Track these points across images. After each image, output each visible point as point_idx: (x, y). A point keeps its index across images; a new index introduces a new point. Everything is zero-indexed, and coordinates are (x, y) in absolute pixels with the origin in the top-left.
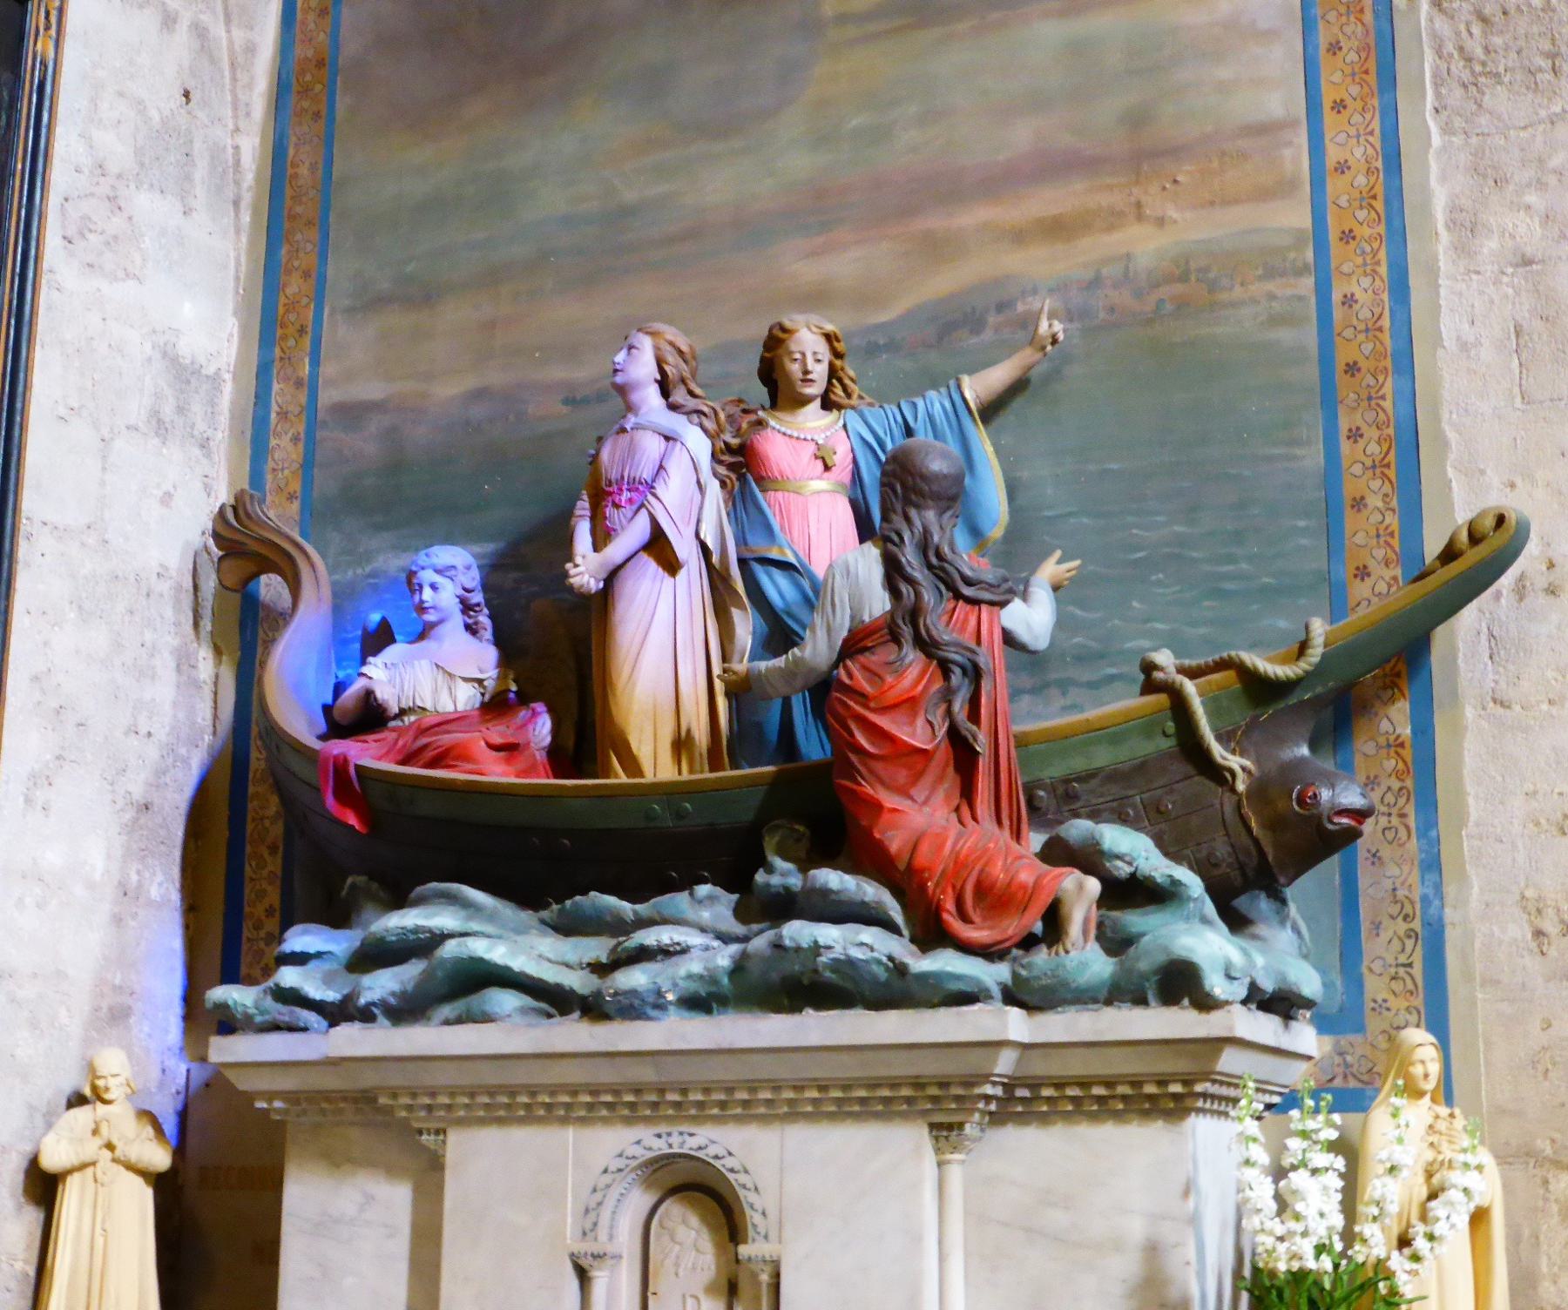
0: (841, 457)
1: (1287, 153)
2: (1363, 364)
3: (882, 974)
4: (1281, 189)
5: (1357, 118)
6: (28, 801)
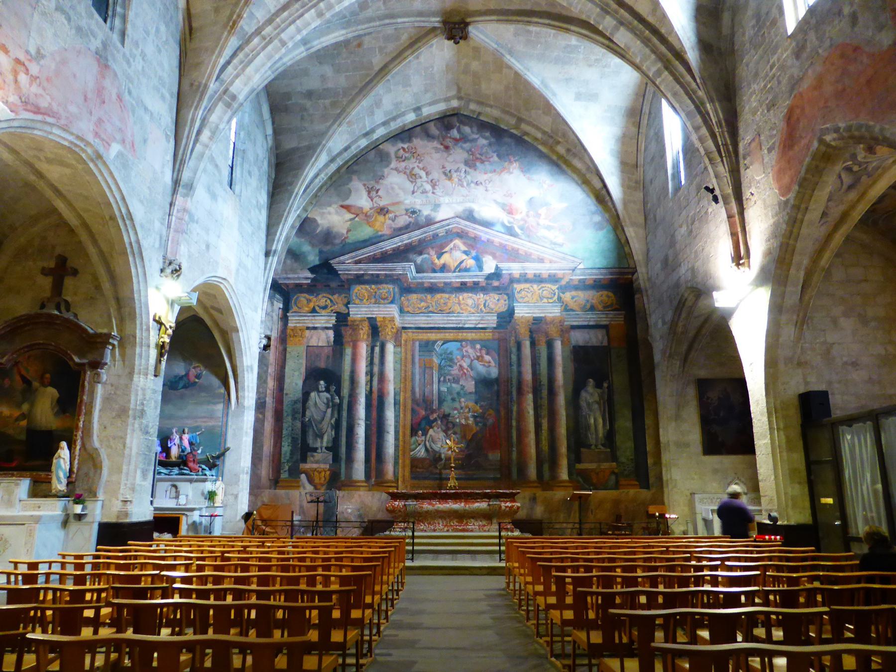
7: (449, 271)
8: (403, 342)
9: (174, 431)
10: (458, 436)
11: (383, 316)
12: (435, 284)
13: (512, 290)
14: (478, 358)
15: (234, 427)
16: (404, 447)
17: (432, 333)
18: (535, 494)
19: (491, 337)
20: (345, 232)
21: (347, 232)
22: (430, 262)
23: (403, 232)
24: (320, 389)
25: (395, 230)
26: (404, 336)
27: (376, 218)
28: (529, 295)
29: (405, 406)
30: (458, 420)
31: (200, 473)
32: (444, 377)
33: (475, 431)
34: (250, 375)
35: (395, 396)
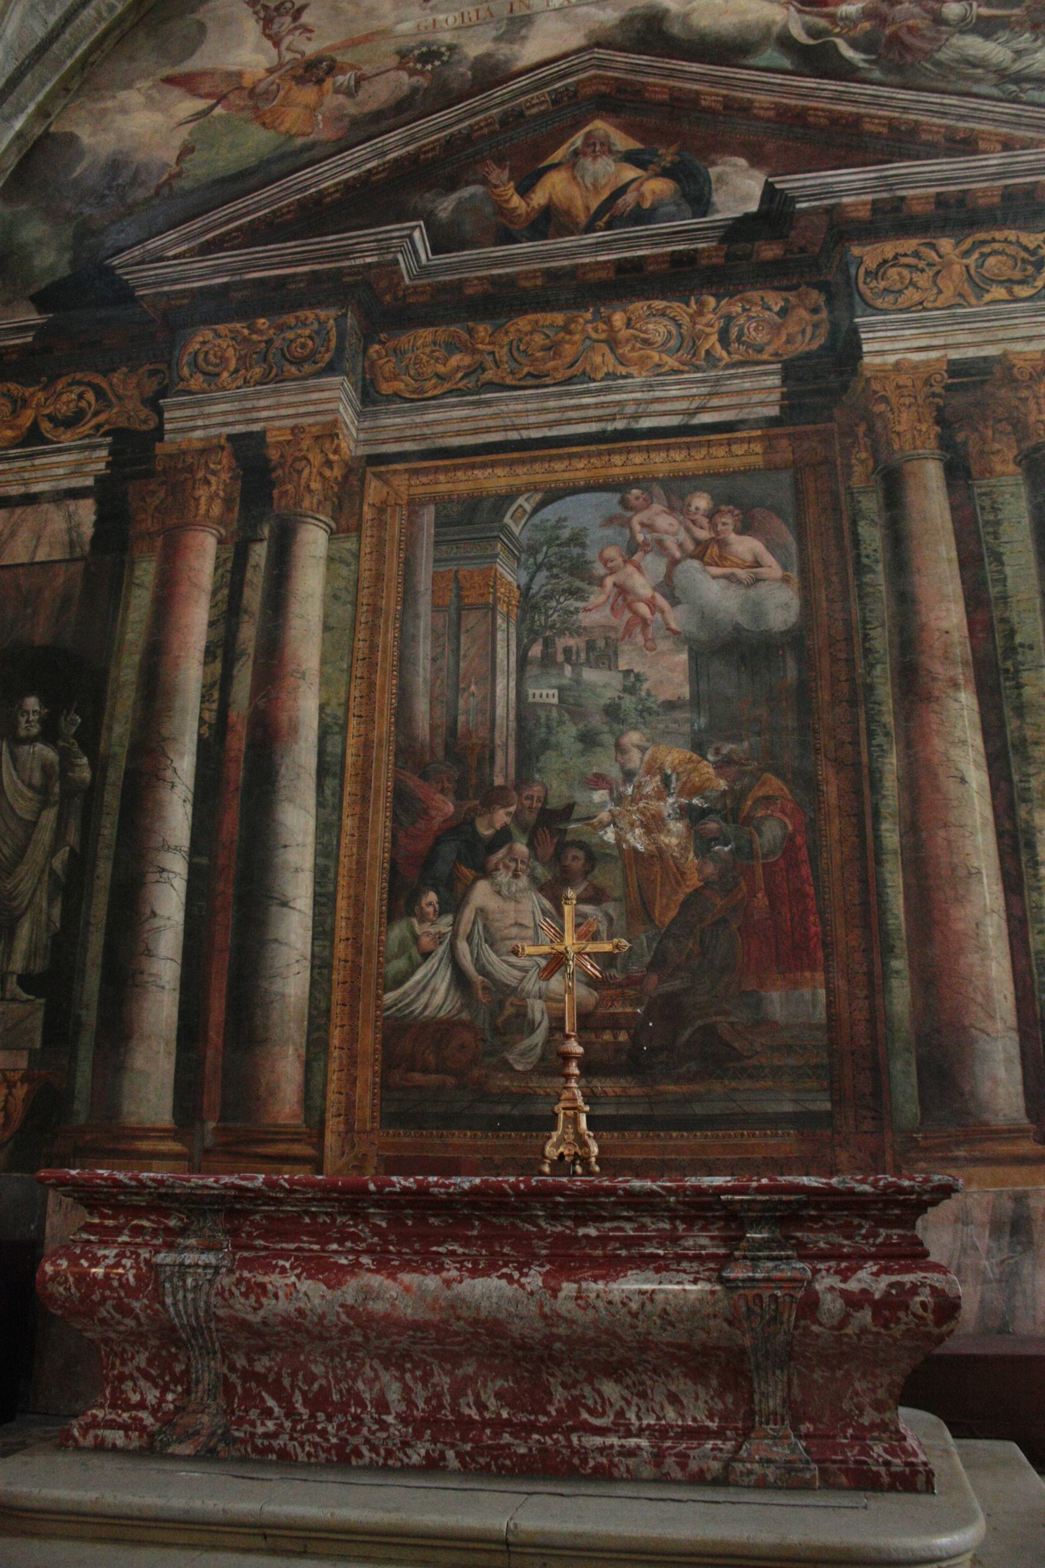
7: (565, 230)
8: (368, 513)
10: (611, 908)
11: (289, 423)
12: (510, 281)
13: (846, 272)
14: (700, 551)
16: (356, 969)
17: (493, 465)
18: (1019, 1199)
19: (757, 461)
20: (170, 156)
21: (179, 160)
22: (488, 209)
23: (384, 124)
24: (23, 733)
25: (355, 122)
26: (374, 491)
27: (286, 96)
28: (923, 280)
29: (365, 781)
30: (610, 836)
32: (548, 643)
33: (694, 881)
35: (322, 738)
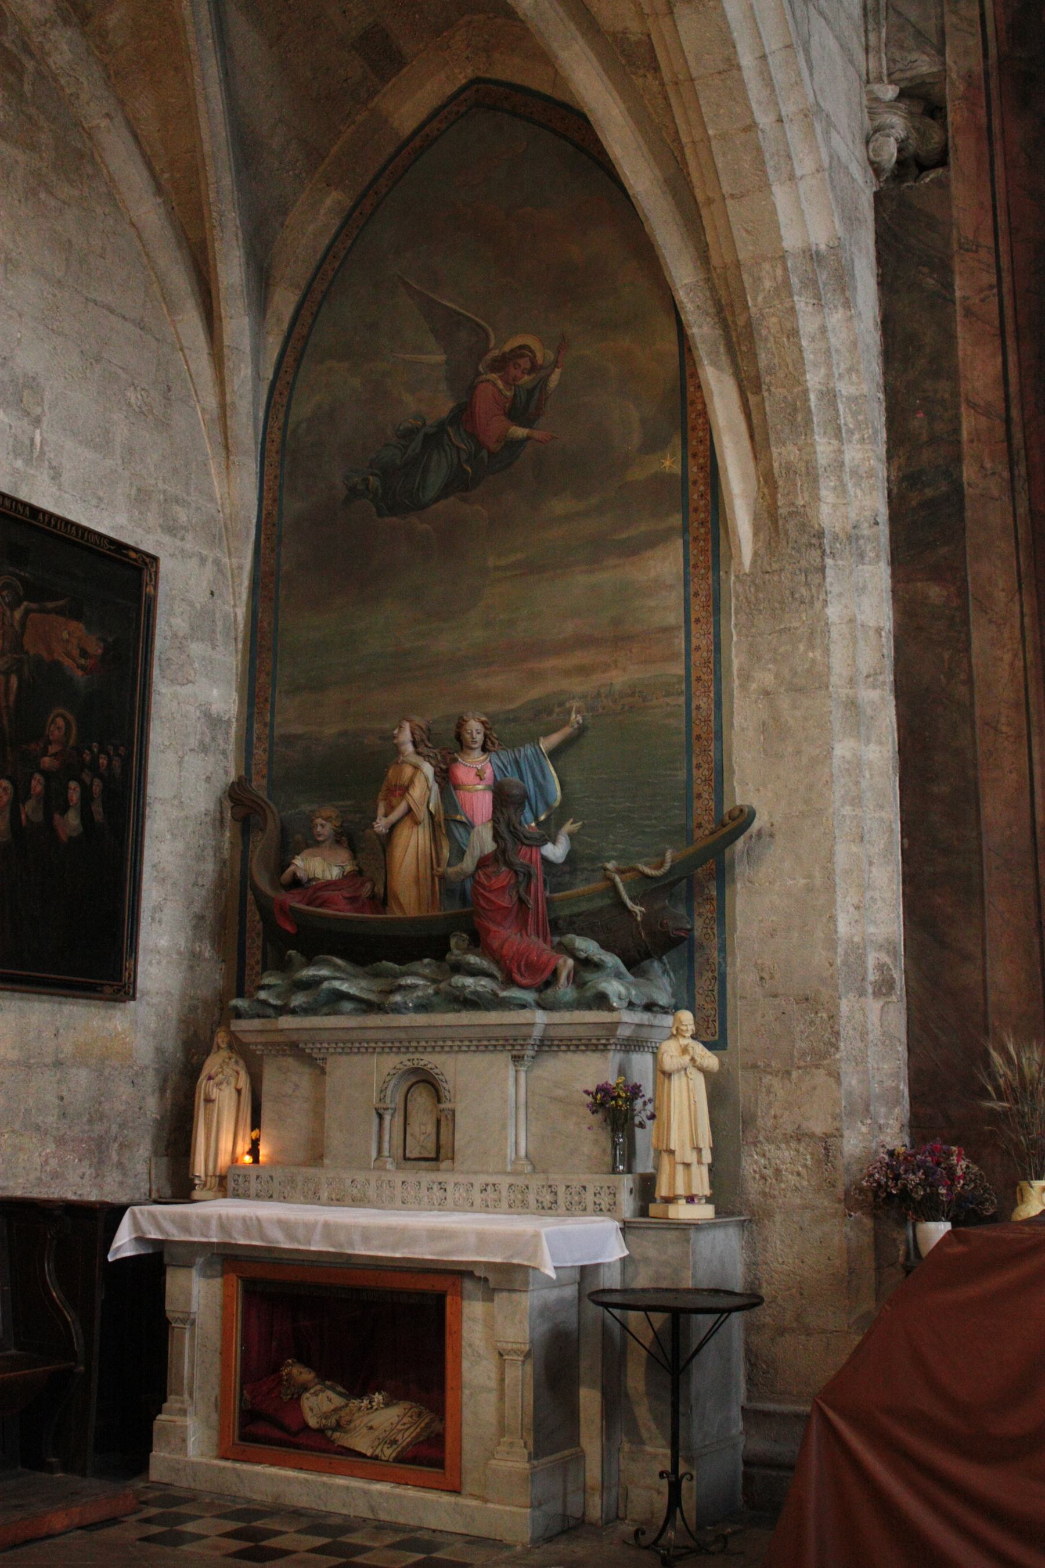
0: (488, 773)
1: (676, 641)
2: (704, 736)
3: (490, 997)
4: (672, 657)
5: (704, 626)
6: (153, 919)
9: (405, 736)
15: (766, 678)
31: (565, 990)
34: (836, 318)
